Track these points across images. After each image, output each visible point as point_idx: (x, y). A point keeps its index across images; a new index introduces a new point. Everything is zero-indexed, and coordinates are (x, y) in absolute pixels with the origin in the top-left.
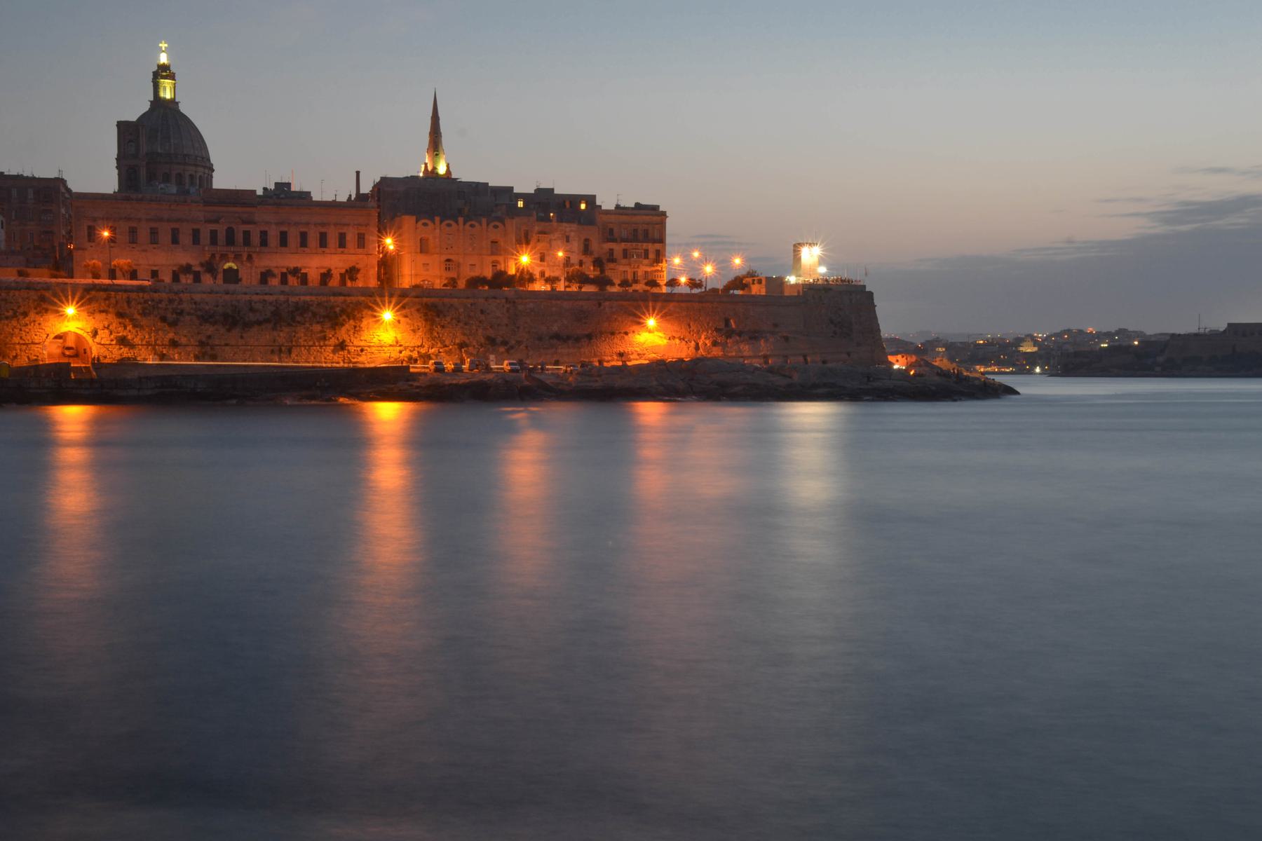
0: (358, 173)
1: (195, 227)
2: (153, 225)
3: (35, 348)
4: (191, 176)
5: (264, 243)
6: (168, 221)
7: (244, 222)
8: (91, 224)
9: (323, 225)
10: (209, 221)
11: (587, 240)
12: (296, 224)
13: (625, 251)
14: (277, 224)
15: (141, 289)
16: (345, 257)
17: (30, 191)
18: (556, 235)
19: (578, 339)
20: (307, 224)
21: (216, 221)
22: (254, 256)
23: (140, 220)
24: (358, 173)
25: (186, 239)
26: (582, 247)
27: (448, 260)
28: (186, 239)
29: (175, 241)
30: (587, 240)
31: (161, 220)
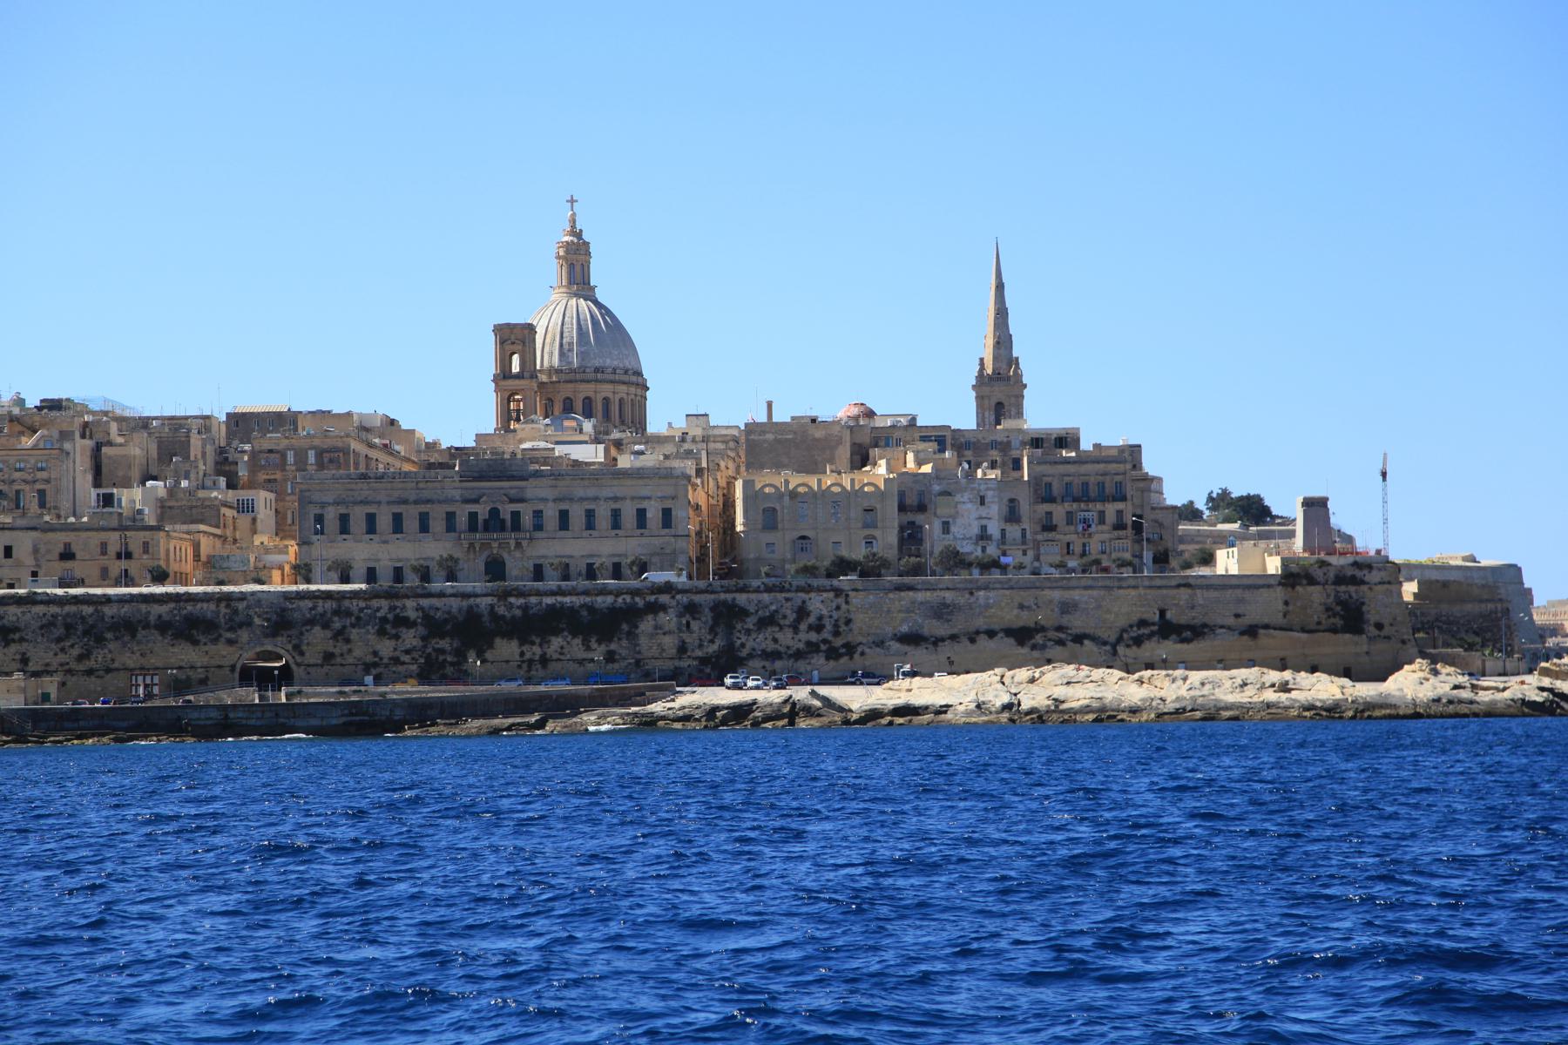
0: (770, 405)
1: (450, 509)
2: (397, 509)
3: (1364, 588)
4: (606, 399)
5: (538, 527)
6: (416, 502)
7: (512, 501)
8: (318, 511)
9: (616, 499)
10: (467, 501)
11: (1012, 501)
12: (582, 499)
13: (1070, 515)
14: (555, 500)
15: (355, 595)
16: (644, 540)
17: (311, 454)
18: (966, 496)
19: (937, 641)
20: (596, 499)
21: (476, 501)
22: (525, 543)
23: (379, 503)
24: (770, 405)
25: (437, 525)
26: (1005, 509)
27: (803, 538)
28: (437, 525)
29: (424, 528)
30: (1012, 501)
31: (405, 502)
